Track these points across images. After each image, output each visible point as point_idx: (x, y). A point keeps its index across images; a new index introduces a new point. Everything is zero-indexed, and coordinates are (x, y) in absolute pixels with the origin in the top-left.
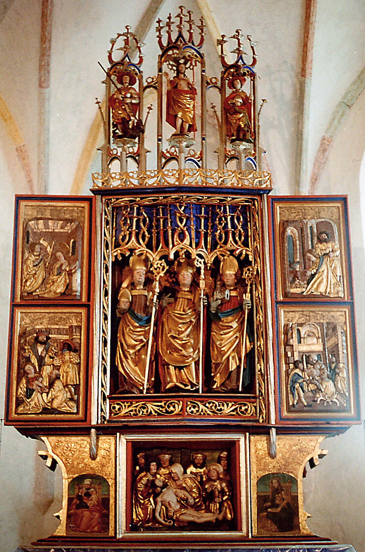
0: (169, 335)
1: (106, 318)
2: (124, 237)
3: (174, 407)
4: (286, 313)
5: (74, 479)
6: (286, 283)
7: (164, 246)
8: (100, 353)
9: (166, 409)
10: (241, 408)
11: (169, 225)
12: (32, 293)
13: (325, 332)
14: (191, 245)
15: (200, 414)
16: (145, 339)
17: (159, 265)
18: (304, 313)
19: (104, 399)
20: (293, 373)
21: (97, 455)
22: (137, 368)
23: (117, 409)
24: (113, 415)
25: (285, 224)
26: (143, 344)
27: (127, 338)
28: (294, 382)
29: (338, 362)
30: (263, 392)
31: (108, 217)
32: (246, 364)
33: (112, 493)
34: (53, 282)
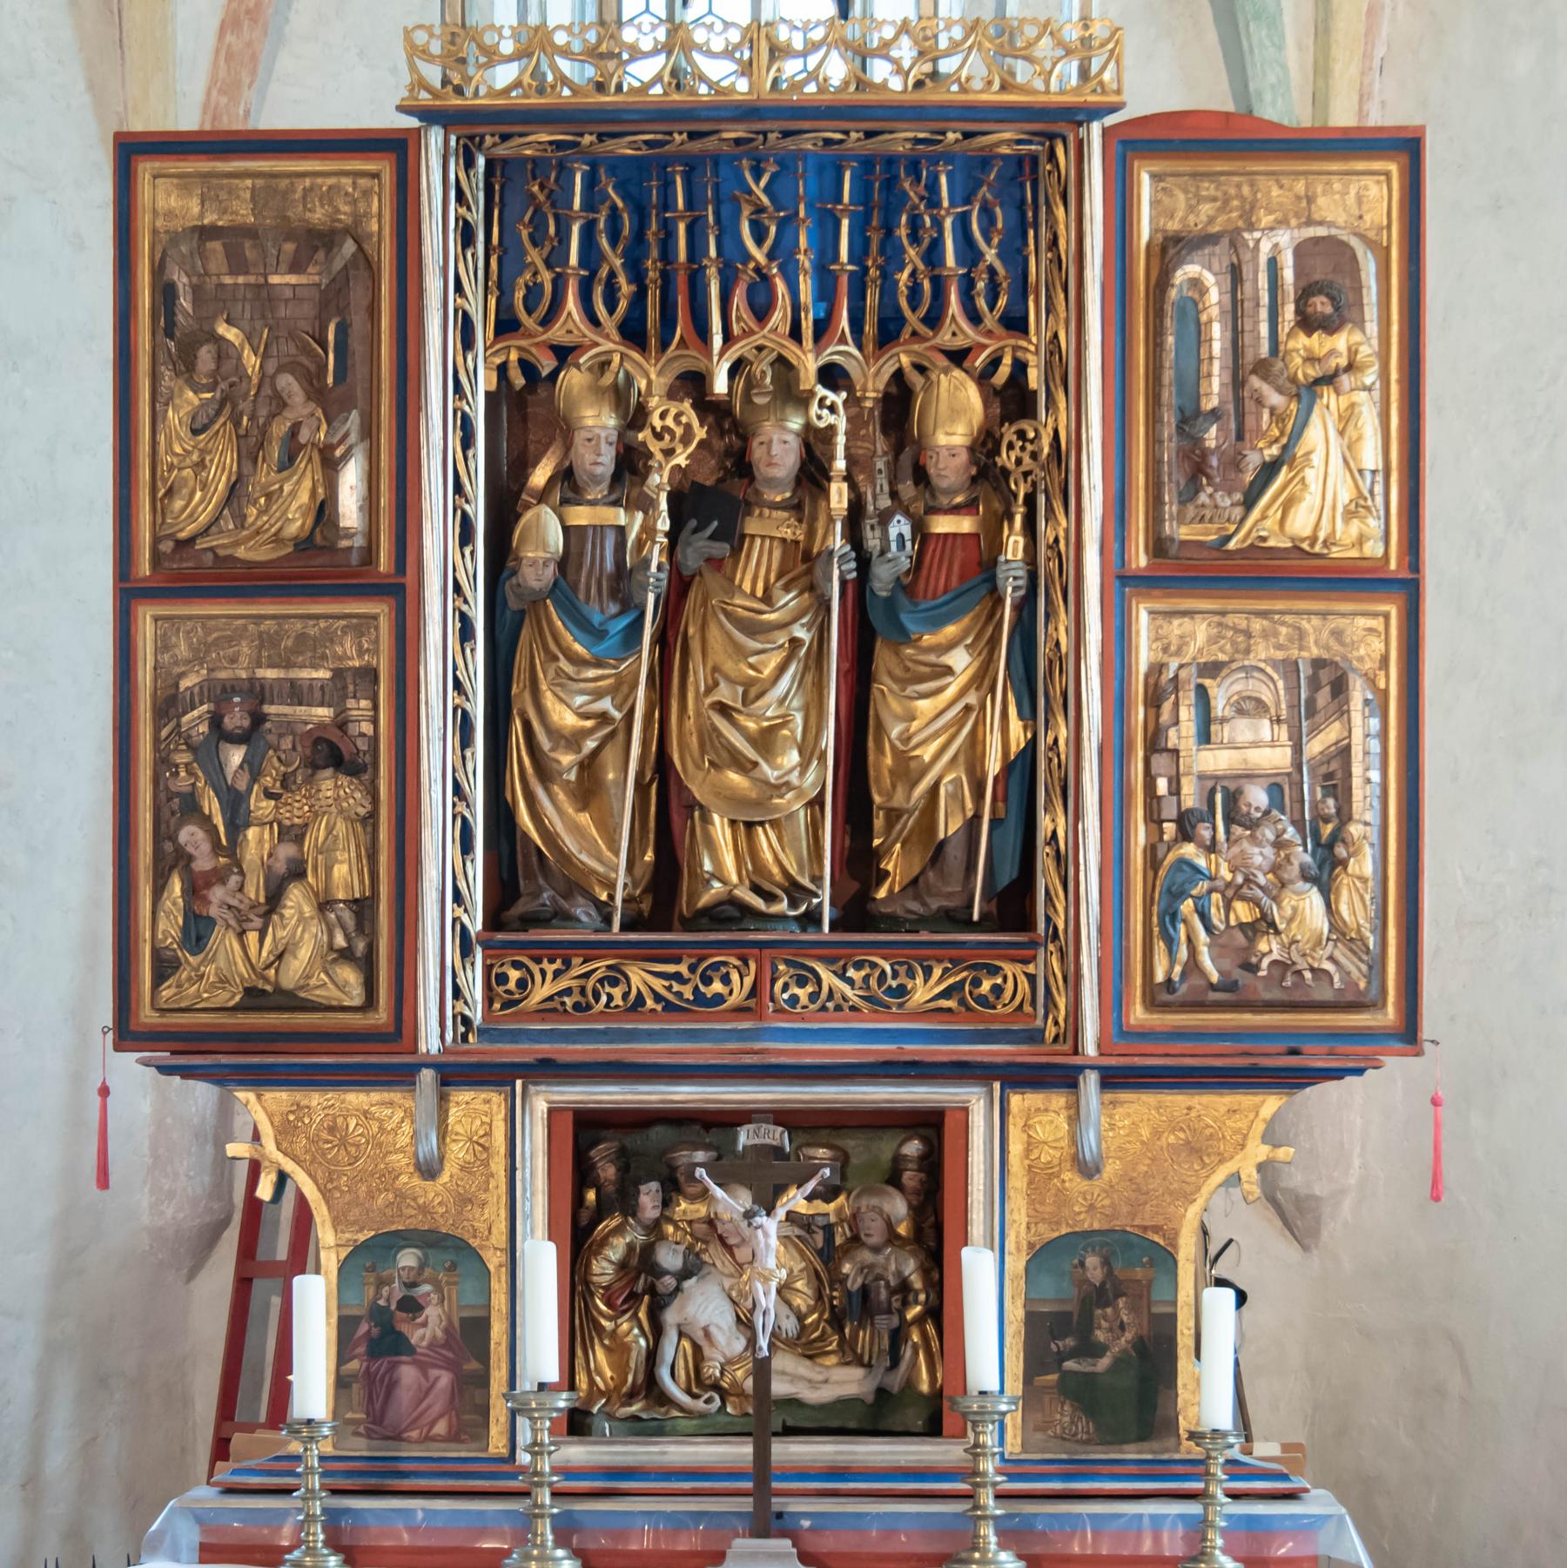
0: (708, 701)
1: (466, 633)
2: (533, 292)
3: (726, 980)
4: (1160, 621)
5: (359, 1250)
6: (1163, 504)
7: (692, 337)
8: (446, 770)
9: (696, 988)
10: (977, 983)
11: (713, 253)
12: (191, 540)
13: (1303, 696)
14: (796, 334)
15: (824, 1008)
16: (619, 708)
17: (669, 422)
18: (1230, 620)
19: (466, 950)
20: (1171, 857)
21: (442, 1159)
22: (584, 818)
23: (512, 985)
24: (497, 1006)
25: (1171, 249)
26: (610, 729)
27: (549, 700)
28: (1177, 895)
29: (1344, 815)
30: (1061, 926)
31: (469, 209)
32: (1005, 800)
33: (499, 1300)
34: (269, 496)
